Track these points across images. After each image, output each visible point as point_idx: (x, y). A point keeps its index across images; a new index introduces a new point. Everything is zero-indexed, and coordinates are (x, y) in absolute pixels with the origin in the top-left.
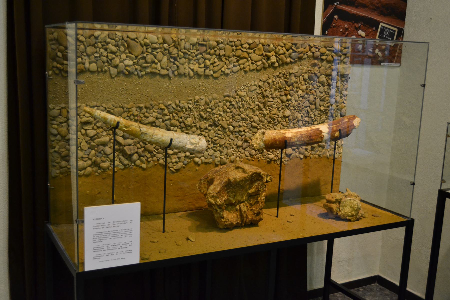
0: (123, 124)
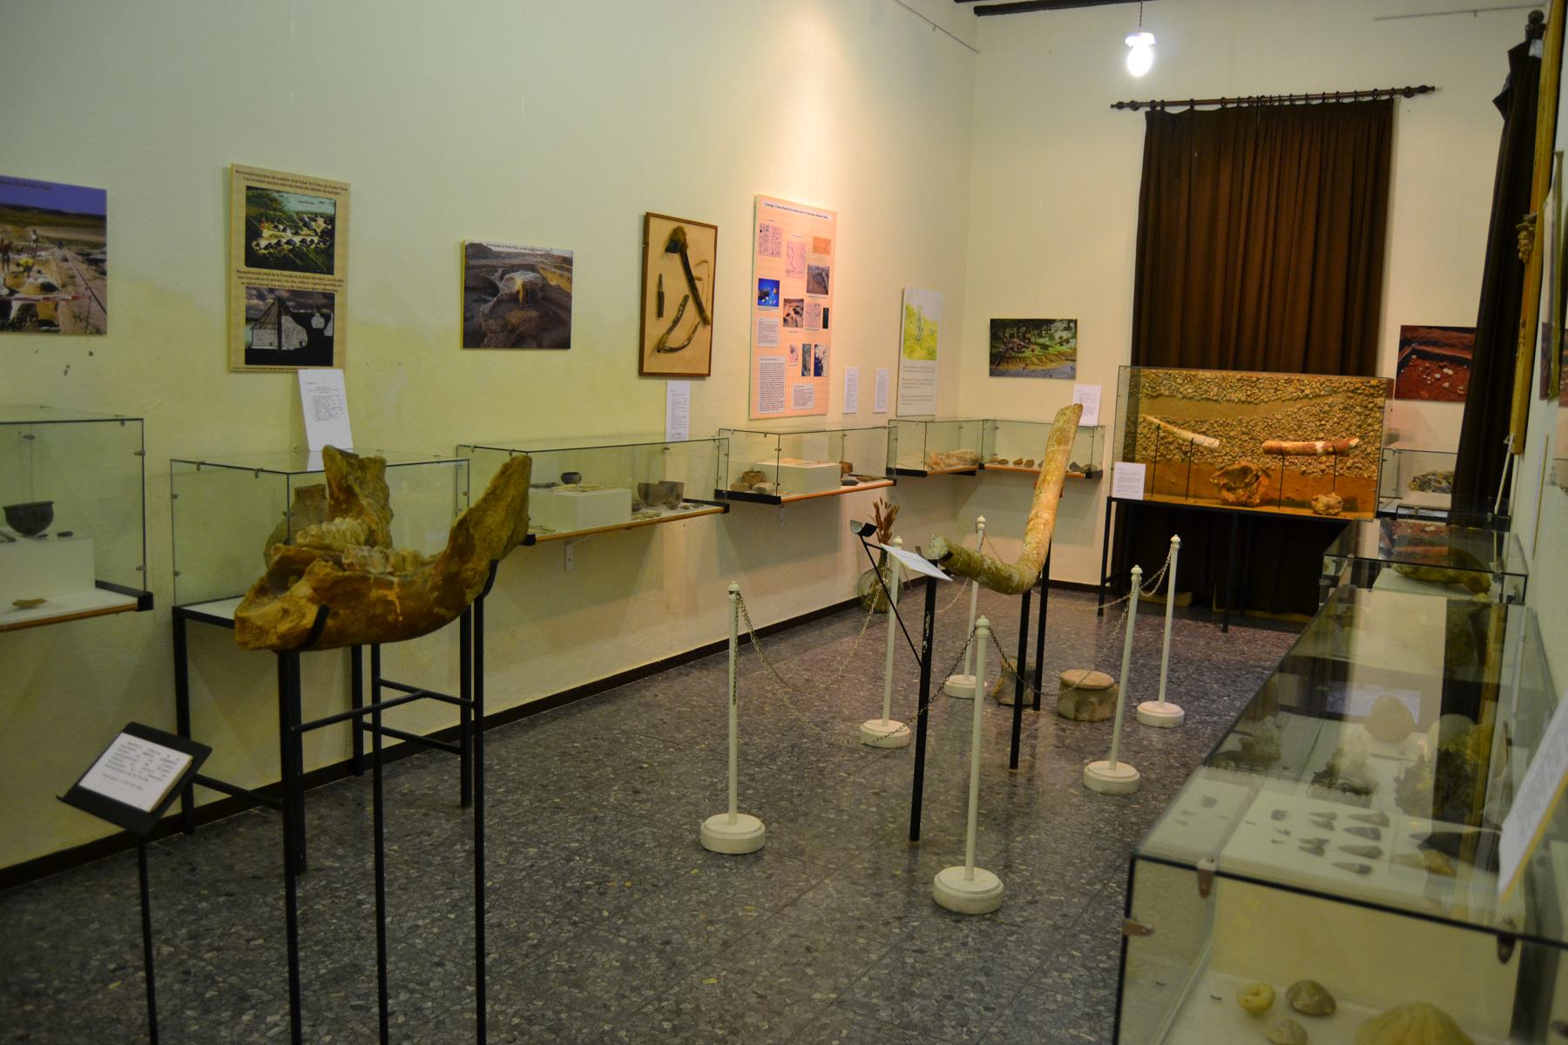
0: (536, 284)
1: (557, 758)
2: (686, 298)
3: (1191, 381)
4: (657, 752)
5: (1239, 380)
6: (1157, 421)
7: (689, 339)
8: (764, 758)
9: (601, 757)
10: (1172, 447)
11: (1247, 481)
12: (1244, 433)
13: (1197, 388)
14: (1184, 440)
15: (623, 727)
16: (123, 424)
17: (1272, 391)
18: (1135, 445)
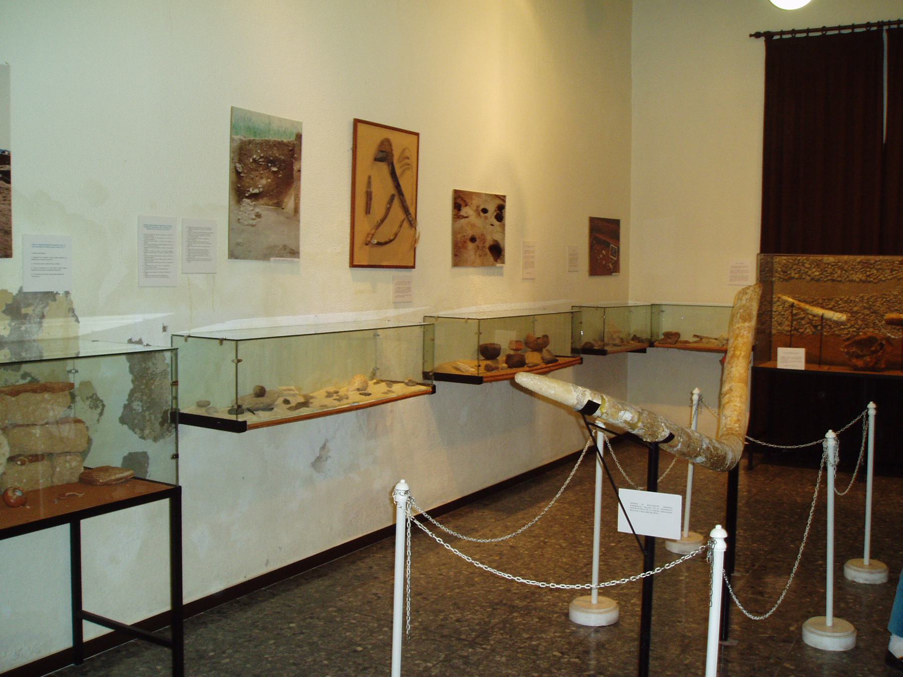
1: (272, 642)
2: (393, 196)
3: (817, 265)
4: (372, 632)
5: (859, 263)
6: (790, 300)
7: (396, 235)
8: (477, 637)
9: (315, 639)
10: (803, 322)
11: (873, 349)
12: (865, 308)
13: (823, 271)
14: (814, 316)
15: (339, 604)
16: (221, 344)
17: (888, 271)
18: (771, 321)
